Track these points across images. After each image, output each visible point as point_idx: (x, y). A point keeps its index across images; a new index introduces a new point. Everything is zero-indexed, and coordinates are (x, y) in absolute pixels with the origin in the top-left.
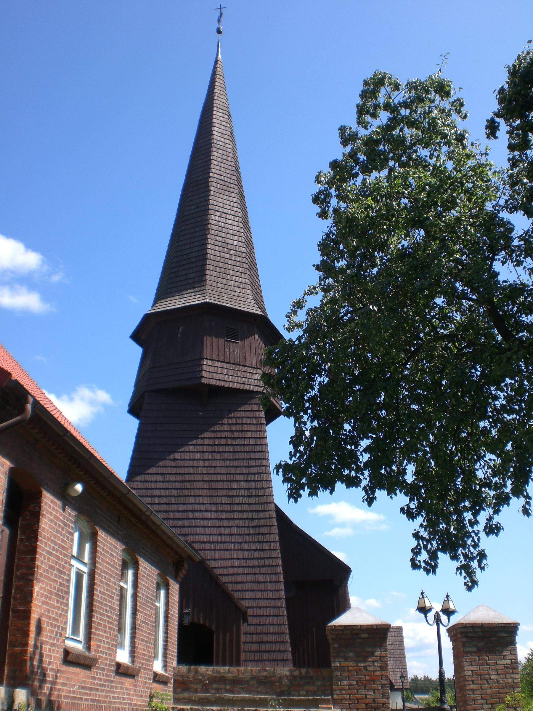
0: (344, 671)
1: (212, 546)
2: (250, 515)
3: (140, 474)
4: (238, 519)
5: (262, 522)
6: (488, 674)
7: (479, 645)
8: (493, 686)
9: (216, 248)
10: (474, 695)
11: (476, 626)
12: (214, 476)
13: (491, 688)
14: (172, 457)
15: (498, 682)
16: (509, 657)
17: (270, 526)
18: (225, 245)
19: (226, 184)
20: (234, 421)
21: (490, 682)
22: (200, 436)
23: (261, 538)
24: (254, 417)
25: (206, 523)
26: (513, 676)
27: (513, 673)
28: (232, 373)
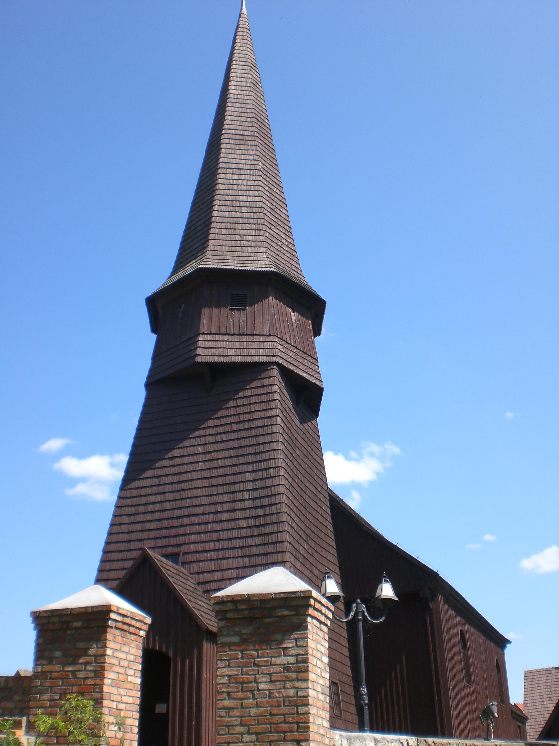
0: (46, 678)
1: (209, 555)
2: (255, 512)
3: (135, 480)
4: (241, 519)
5: (268, 520)
6: (256, 681)
7: (244, 631)
8: (261, 702)
9: (223, 208)
10: (229, 717)
11: (238, 600)
12: (215, 471)
13: (257, 706)
14: (169, 455)
15: (270, 695)
16: (293, 652)
17: (277, 523)
18: (236, 204)
19: (241, 137)
20: (241, 402)
21: (256, 696)
22: (203, 426)
23: (266, 539)
24: (264, 394)
25: (202, 528)
26: (297, 684)
27: (298, 680)
28: (237, 345)
